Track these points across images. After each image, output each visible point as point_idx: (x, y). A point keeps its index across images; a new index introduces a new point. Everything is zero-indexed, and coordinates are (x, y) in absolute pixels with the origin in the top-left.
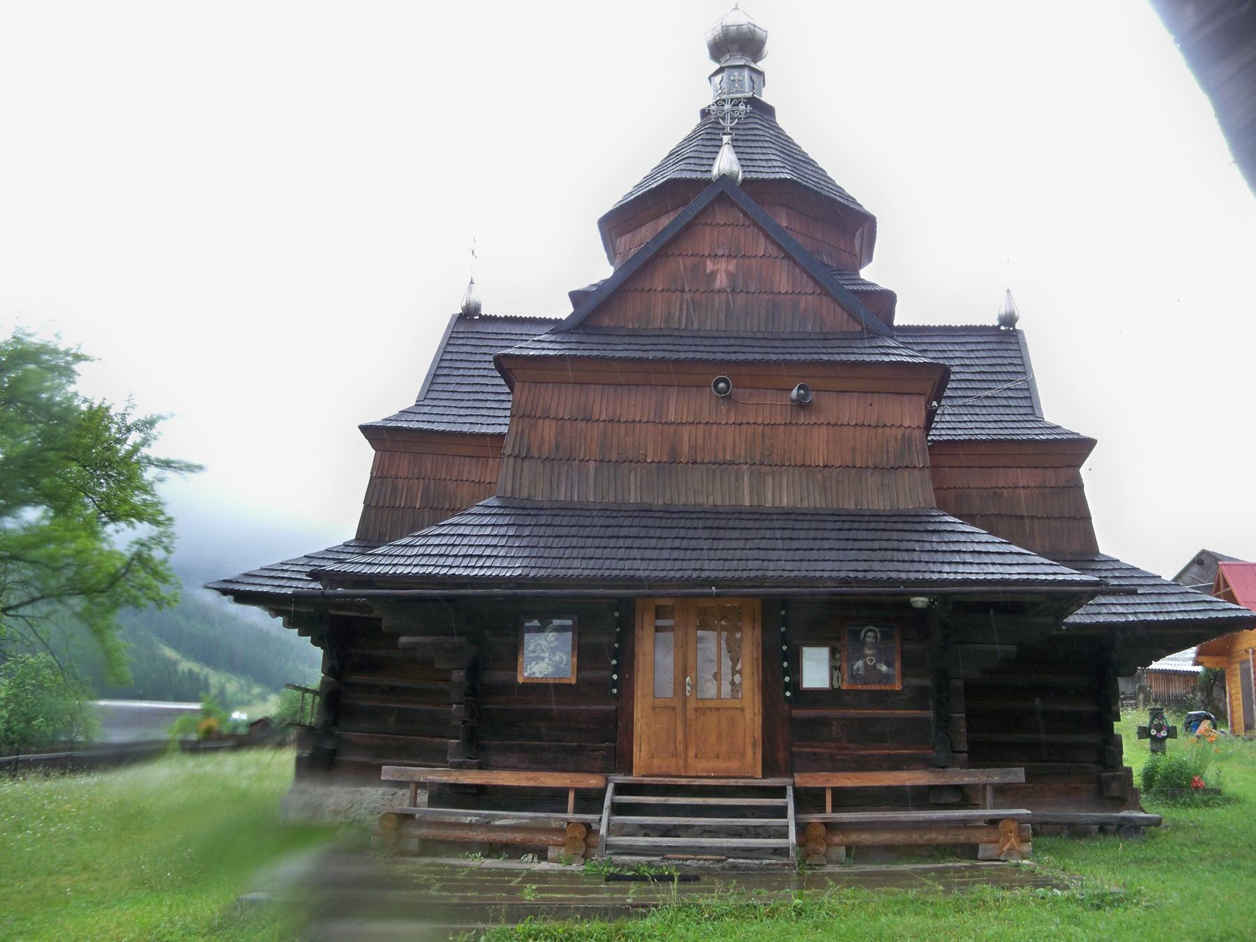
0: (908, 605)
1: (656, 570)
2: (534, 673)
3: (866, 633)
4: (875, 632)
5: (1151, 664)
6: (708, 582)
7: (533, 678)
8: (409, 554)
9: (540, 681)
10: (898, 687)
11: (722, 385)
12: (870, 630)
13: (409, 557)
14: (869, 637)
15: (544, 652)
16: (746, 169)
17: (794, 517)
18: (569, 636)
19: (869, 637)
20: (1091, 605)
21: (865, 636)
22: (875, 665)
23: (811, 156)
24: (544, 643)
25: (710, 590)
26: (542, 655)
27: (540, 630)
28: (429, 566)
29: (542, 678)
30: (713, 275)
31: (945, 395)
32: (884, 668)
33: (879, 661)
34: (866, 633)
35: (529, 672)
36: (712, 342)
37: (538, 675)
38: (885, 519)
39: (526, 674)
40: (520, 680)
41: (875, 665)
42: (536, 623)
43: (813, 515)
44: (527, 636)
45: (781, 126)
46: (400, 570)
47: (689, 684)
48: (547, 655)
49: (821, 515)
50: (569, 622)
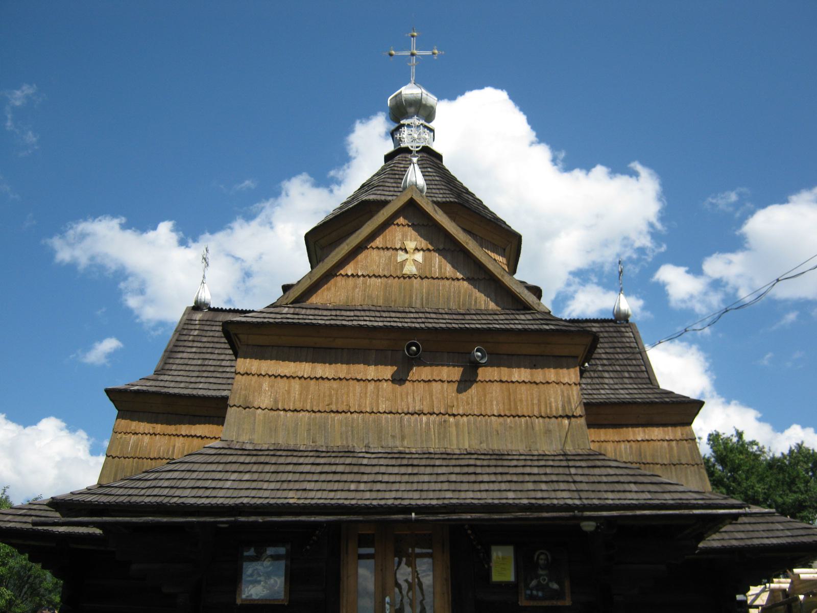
0: (578, 527)
1: (361, 499)
2: (251, 595)
3: (539, 556)
4: (546, 554)
5: (749, 590)
6: (407, 510)
7: (250, 600)
8: (142, 486)
9: (256, 602)
10: (568, 602)
11: (414, 348)
12: (542, 553)
13: (143, 489)
14: (542, 559)
15: (260, 576)
16: (429, 182)
17: (475, 456)
18: (282, 564)
19: (542, 559)
20: (709, 540)
21: (538, 558)
22: (547, 584)
23: (471, 190)
24: (261, 568)
25: (409, 516)
26: (259, 579)
27: (257, 558)
28: (160, 496)
29: (258, 600)
30: (403, 264)
31: (593, 357)
32: (555, 586)
33: (550, 580)
34: (539, 556)
35: (247, 594)
36: (404, 315)
37: (254, 597)
38: (552, 458)
39: (244, 596)
40: (239, 602)
41: (547, 584)
42: (251, 552)
43: (491, 455)
44: (245, 564)
45: (447, 167)
46: (134, 499)
47: (388, 603)
48: (262, 578)
49: (497, 455)
50: (282, 550)
